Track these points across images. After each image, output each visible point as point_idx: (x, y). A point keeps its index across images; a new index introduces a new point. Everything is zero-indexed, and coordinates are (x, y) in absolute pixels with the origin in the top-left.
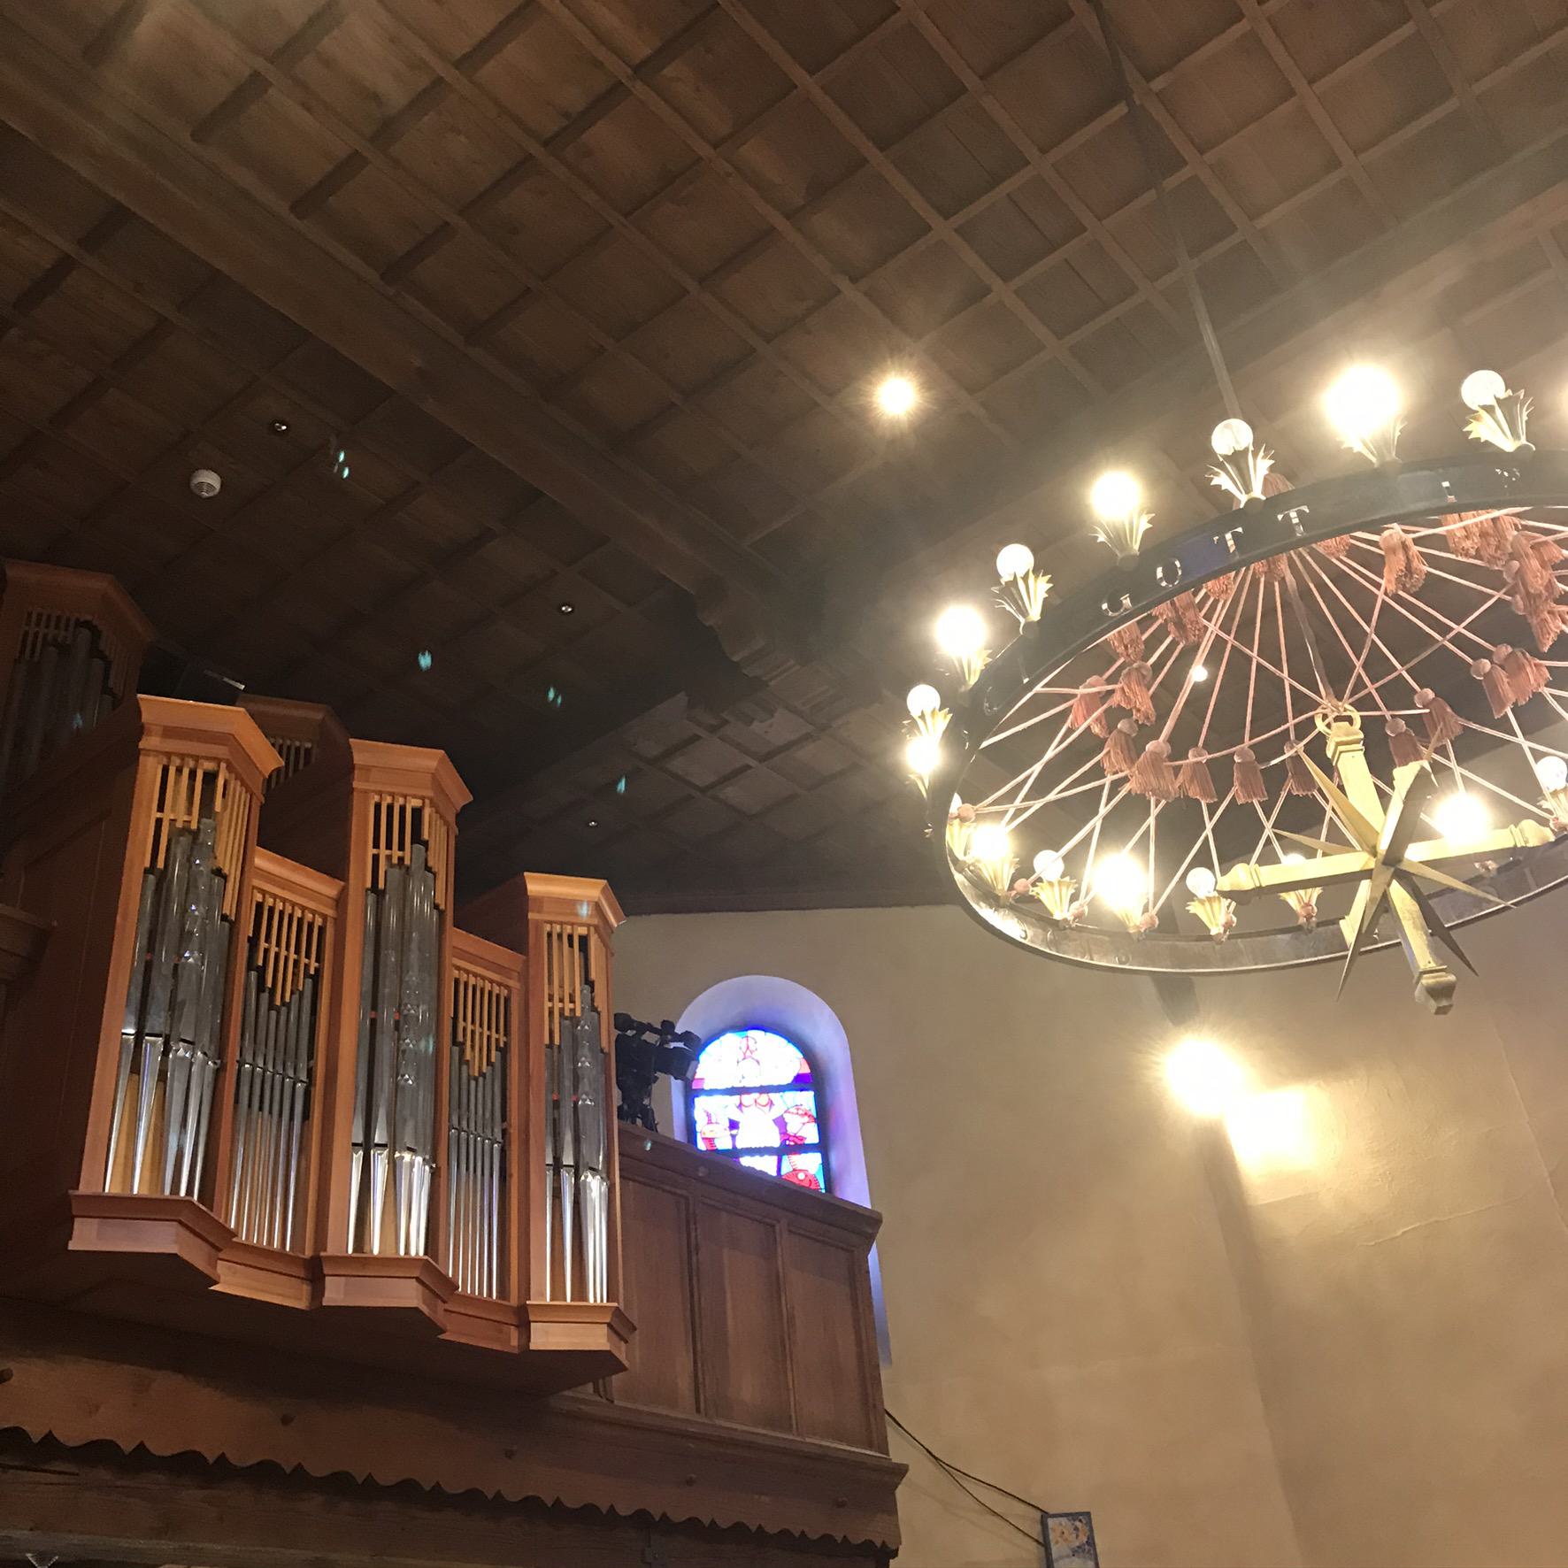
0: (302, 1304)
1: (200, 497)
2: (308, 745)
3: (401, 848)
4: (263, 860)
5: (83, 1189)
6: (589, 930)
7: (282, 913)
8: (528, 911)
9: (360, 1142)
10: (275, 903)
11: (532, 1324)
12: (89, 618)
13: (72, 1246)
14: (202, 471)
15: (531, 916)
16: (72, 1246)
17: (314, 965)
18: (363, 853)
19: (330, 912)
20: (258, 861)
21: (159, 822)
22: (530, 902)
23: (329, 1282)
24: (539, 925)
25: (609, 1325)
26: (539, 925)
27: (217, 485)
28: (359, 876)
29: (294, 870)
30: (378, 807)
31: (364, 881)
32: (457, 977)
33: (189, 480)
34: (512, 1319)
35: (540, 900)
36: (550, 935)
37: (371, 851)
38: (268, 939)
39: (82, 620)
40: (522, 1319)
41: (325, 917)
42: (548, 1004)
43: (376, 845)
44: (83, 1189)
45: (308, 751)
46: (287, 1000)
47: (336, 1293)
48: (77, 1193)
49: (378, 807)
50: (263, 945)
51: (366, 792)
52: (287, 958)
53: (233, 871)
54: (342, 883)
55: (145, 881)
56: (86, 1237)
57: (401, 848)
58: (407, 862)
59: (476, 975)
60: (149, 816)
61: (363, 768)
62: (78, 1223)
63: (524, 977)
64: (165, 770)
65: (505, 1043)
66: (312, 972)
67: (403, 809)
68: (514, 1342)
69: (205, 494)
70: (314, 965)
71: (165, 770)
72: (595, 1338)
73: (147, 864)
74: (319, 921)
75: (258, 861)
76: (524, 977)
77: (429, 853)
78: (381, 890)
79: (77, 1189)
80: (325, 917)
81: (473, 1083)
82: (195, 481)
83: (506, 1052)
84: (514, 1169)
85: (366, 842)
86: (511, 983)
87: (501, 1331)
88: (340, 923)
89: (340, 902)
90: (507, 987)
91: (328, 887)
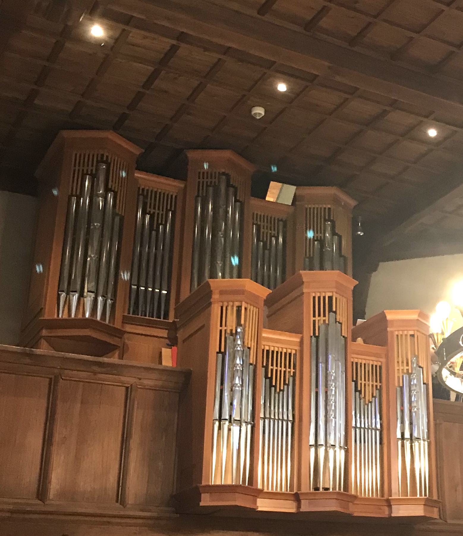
0: (293, 510)
1: (256, 119)
2: (329, 206)
3: (324, 316)
4: (266, 334)
5: (204, 483)
6: (414, 332)
7: (277, 352)
8: (387, 327)
9: (313, 444)
10: (274, 349)
11: (393, 506)
12: (223, 171)
13: (201, 504)
14: (256, 107)
15: (388, 329)
16: (201, 504)
17: (292, 370)
18: (309, 319)
19: (297, 348)
20: (264, 335)
21: (221, 331)
22: (388, 323)
23: (303, 502)
24: (392, 332)
25: (424, 505)
26: (392, 332)
27: (263, 114)
28: (308, 331)
29: (280, 335)
30: (314, 298)
31: (310, 333)
32: (357, 362)
33: (250, 111)
34: (385, 503)
35: (392, 321)
36: (398, 336)
37: (312, 319)
38: (272, 365)
39: (221, 172)
40: (389, 503)
41: (296, 350)
42: (396, 368)
43: (314, 316)
44: (204, 483)
45: (329, 208)
46: (282, 388)
47: (305, 507)
48: (201, 485)
49: (314, 298)
50: (270, 367)
51: (309, 293)
52: (281, 371)
53: (253, 344)
54: (301, 335)
55: (217, 356)
56: (206, 501)
57: (324, 316)
58: (327, 322)
59: (364, 359)
60: (217, 329)
61: (307, 282)
62: (203, 495)
63: (387, 357)
64: (222, 308)
65: (380, 386)
66: (292, 374)
67: (324, 298)
68: (387, 513)
69: (258, 118)
70: (292, 370)
71: (222, 308)
72: (418, 511)
73: (218, 350)
74: (294, 352)
75: (264, 335)
76: (387, 357)
77: (337, 315)
78: (317, 336)
79: (201, 483)
80: (296, 350)
81: (366, 406)
82: (253, 113)
83: (381, 390)
84: (385, 441)
85: (310, 314)
86: (381, 360)
87: (380, 509)
88: (302, 351)
89: (301, 343)
90: (380, 361)
91: (295, 339)
